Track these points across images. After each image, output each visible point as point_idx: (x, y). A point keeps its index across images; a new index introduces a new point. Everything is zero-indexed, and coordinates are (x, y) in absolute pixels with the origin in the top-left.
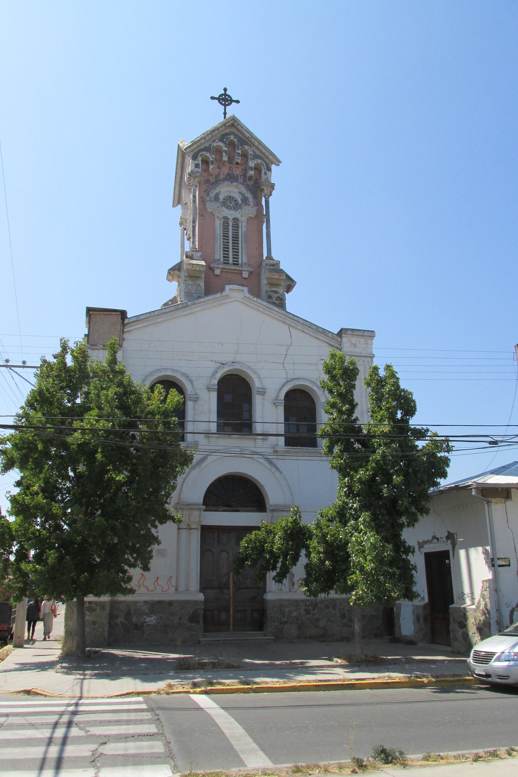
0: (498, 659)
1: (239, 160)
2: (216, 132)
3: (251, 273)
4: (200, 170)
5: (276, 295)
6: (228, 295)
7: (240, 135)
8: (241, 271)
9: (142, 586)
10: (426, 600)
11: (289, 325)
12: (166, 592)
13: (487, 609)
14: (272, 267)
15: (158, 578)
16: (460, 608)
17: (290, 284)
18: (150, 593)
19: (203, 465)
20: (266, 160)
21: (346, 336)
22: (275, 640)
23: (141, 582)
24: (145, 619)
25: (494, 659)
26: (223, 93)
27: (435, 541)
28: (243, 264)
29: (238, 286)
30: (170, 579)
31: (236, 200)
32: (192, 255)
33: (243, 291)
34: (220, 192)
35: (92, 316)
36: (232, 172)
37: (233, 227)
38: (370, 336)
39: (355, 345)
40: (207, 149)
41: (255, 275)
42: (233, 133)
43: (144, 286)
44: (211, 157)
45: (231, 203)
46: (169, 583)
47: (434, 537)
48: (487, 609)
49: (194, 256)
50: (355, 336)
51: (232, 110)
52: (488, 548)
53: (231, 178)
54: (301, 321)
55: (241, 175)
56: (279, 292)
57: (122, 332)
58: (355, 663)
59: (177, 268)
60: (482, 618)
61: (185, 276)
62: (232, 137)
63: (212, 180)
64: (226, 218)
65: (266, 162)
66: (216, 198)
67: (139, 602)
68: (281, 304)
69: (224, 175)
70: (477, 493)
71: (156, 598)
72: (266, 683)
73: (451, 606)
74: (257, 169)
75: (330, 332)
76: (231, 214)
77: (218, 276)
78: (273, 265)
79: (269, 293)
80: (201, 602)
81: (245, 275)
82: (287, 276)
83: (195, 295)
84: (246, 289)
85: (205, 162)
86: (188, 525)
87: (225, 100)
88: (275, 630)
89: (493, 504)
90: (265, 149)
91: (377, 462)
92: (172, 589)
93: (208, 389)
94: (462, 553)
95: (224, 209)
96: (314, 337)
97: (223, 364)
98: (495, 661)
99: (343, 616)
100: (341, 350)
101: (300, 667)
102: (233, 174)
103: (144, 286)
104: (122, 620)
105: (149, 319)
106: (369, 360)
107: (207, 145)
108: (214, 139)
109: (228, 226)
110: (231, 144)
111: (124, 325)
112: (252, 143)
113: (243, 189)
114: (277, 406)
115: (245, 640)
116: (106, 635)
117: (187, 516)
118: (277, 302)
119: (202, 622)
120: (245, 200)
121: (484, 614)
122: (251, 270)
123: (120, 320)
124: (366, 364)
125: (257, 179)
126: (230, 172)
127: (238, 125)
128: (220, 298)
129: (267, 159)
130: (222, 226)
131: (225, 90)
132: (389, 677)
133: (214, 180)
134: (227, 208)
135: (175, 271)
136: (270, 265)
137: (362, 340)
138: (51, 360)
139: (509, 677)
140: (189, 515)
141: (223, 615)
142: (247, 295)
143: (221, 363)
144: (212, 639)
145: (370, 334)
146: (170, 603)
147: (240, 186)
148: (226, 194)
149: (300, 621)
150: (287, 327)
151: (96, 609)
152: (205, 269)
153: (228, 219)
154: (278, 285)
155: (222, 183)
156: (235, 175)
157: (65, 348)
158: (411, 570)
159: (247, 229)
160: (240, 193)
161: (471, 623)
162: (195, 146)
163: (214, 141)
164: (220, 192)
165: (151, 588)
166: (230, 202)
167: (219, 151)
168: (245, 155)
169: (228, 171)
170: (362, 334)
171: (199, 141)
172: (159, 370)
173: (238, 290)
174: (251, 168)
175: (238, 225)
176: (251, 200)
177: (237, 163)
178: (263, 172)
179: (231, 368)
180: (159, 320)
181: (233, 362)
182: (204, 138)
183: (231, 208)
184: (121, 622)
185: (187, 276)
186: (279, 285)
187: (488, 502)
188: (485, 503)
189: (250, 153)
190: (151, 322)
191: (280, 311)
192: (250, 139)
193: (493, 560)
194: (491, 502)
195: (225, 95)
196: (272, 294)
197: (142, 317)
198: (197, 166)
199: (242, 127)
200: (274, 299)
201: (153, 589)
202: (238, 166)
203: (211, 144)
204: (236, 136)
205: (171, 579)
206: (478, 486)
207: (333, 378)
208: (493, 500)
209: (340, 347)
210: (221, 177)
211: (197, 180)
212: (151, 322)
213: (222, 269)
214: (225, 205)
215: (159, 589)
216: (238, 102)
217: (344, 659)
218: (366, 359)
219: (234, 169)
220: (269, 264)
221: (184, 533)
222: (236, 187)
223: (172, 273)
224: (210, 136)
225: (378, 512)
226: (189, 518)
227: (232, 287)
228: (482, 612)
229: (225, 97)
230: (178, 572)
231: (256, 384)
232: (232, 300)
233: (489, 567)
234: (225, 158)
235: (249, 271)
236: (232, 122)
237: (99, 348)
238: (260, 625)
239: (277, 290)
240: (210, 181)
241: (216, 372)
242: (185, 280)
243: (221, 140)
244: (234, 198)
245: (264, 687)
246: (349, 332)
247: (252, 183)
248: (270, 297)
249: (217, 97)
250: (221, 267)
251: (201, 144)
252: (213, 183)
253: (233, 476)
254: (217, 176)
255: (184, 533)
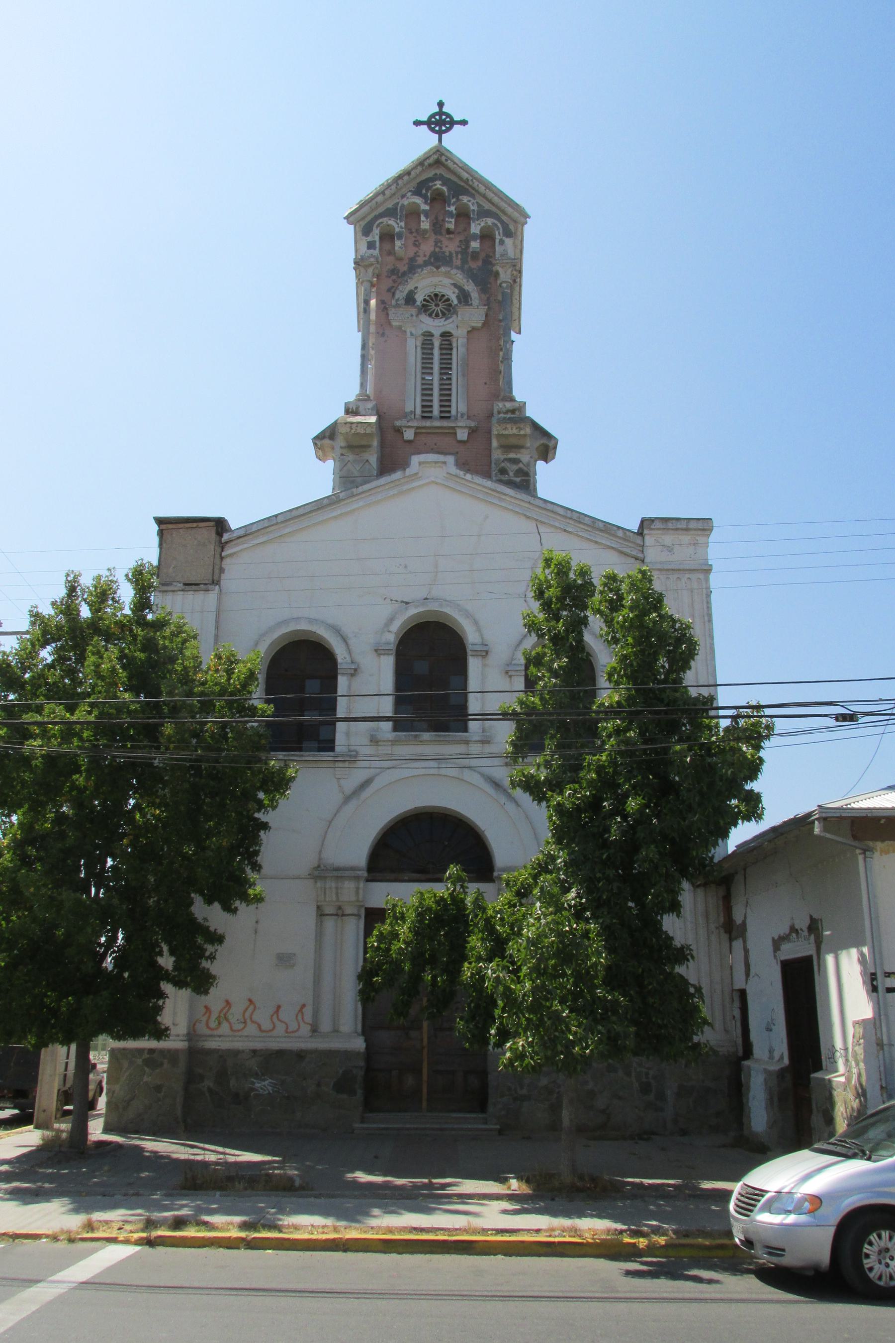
0: (769, 1207)
1: (451, 224)
2: (406, 178)
3: (473, 431)
4: (376, 252)
5: (515, 467)
6: (417, 474)
7: (453, 178)
8: (453, 428)
9: (248, 1021)
10: (786, 1061)
11: (536, 520)
12: (293, 1035)
13: (861, 1085)
14: (509, 415)
15: (279, 1007)
16: (824, 1079)
17: (546, 447)
18: (264, 1034)
19: (366, 794)
20: (504, 218)
21: (652, 532)
22: (500, 1132)
23: (247, 1014)
24: (253, 1083)
25: (759, 1204)
26: (437, 110)
27: (794, 935)
28: (459, 415)
29: (436, 456)
30: (301, 1010)
31: (448, 300)
32: (357, 408)
33: (445, 463)
34: (416, 288)
35: (165, 532)
36: (441, 248)
37: (441, 349)
38: (704, 530)
39: (670, 549)
40: (391, 212)
41: (480, 433)
42: (441, 177)
43: (266, 473)
44: (398, 226)
45: (437, 305)
46: (300, 1017)
47: (793, 929)
48: (861, 1085)
49: (361, 409)
50: (671, 532)
51: (453, 141)
52: (865, 950)
53: (438, 260)
54: (561, 512)
55: (457, 253)
56: (522, 459)
57: (218, 556)
58: (548, 1193)
59: (327, 434)
60: (855, 1104)
61: (341, 448)
62: (438, 185)
63: (403, 268)
64: (428, 335)
65: (502, 222)
66: (410, 299)
67: (243, 1051)
68: (524, 482)
69: (425, 256)
70: (825, 829)
71: (274, 1045)
72: (296, 1228)
73: (812, 1075)
74: (487, 236)
75: (619, 528)
76: (436, 326)
77: (409, 442)
78: (513, 411)
79: (503, 465)
80: (358, 1053)
81: (462, 435)
82: (536, 426)
83: (359, 480)
84: (451, 459)
85: (388, 237)
86: (340, 908)
87: (440, 122)
88: (503, 1113)
89: (877, 855)
90: (499, 197)
91: (600, 769)
92: (305, 1030)
93: (376, 651)
94: (830, 959)
95: (424, 318)
96: (587, 539)
97: (407, 603)
98: (762, 1210)
99: (645, 1088)
100: (643, 561)
101: (422, 1195)
102: (444, 253)
103: (266, 473)
104: (211, 1085)
105: (268, 530)
106: (701, 576)
107: (390, 206)
108: (404, 191)
109: (432, 349)
110: (438, 199)
111: (222, 546)
112: (474, 189)
113: (459, 277)
114: (510, 676)
115: (441, 1129)
116: (179, 1112)
117: (334, 890)
118: (518, 480)
119: (360, 1092)
120: (464, 298)
121: (858, 1096)
122: (473, 424)
123: (214, 535)
124: (695, 586)
125: (488, 256)
126: (437, 250)
127: (446, 160)
128: (402, 481)
129: (506, 219)
130: (419, 349)
131: (441, 104)
132: (575, 1231)
133: (405, 268)
134: (430, 315)
135: (325, 440)
136: (507, 412)
137: (686, 538)
138: (47, 610)
139: (783, 1250)
140: (337, 888)
141: (410, 1081)
142: (454, 470)
143: (402, 602)
144: (375, 1126)
145: (704, 526)
146: (300, 1055)
147: (454, 271)
148: (430, 290)
149: (555, 1095)
150: (532, 526)
151: (162, 1064)
152: (374, 430)
153: (433, 336)
154: (518, 447)
155: (419, 270)
156: (447, 254)
157: (72, 590)
158: (692, 996)
159: (468, 349)
160: (455, 285)
161: (840, 1113)
162: (366, 209)
163: (403, 196)
164: (416, 288)
165: (267, 1025)
166: (437, 306)
167: (413, 214)
168: (463, 216)
169: (432, 249)
170: (684, 527)
171: (372, 199)
172: (285, 622)
173: (436, 463)
174: (474, 237)
175: (451, 344)
176: (475, 295)
177: (449, 232)
178: (497, 241)
179: (421, 609)
180: (288, 530)
181: (426, 599)
182: (383, 193)
183: (437, 315)
184: (210, 1090)
185: (345, 448)
186: (522, 447)
187: (864, 851)
188: (858, 851)
189: (472, 208)
190: (271, 536)
191: (519, 496)
192: (471, 183)
193: (873, 977)
194: (871, 850)
195: (441, 113)
196: (507, 465)
197: (254, 529)
198: (371, 245)
199: (455, 163)
200: (511, 474)
201: (271, 1027)
202: (451, 236)
203: (398, 203)
204: (446, 182)
205: (304, 1010)
206: (824, 815)
207: (546, 606)
208: (879, 845)
209: (640, 555)
210: (420, 260)
211: (370, 270)
212: (271, 536)
213: (418, 428)
214: (425, 311)
215: (280, 1029)
216: (464, 123)
217: (528, 1181)
218: (694, 576)
219: (445, 242)
220: (504, 410)
221: (329, 924)
222: (447, 275)
223: (319, 443)
224: (393, 187)
225: (598, 875)
226: (337, 894)
227: (423, 457)
228: (854, 1092)
229: (441, 118)
230: (317, 996)
231: (471, 637)
232: (427, 481)
233: (867, 991)
234: (425, 225)
235: (470, 428)
236: (435, 157)
237: (176, 589)
238: (478, 1100)
239: (518, 456)
240: (398, 271)
241: (391, 620)
242: (342, 455)
243: (417, 192)
244: (443, 296)
245: (268, 1238)
246: (658, 525)
247: (480, 263)
248: (503, 471)
249: (425, 119)
250: (415, 424)
251: (378, 205)
252: (404, 274)
253: (431, 814)
254: (412, 260)
255: (329, 924)
